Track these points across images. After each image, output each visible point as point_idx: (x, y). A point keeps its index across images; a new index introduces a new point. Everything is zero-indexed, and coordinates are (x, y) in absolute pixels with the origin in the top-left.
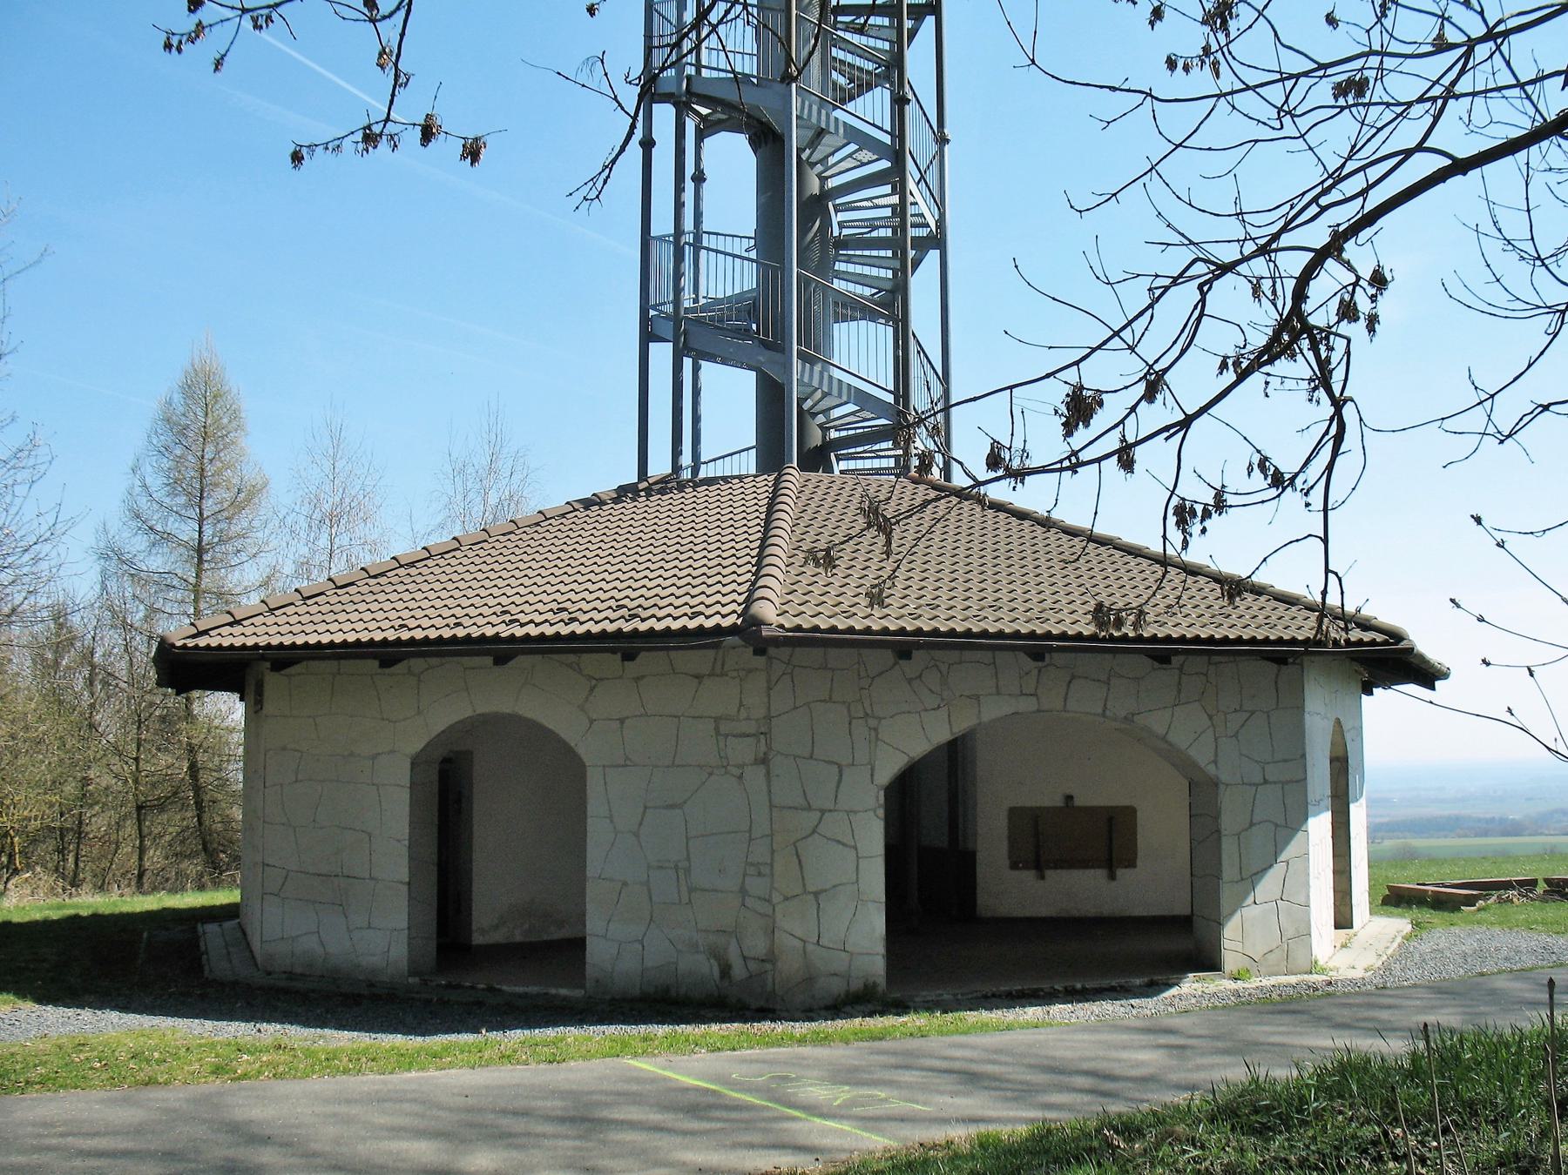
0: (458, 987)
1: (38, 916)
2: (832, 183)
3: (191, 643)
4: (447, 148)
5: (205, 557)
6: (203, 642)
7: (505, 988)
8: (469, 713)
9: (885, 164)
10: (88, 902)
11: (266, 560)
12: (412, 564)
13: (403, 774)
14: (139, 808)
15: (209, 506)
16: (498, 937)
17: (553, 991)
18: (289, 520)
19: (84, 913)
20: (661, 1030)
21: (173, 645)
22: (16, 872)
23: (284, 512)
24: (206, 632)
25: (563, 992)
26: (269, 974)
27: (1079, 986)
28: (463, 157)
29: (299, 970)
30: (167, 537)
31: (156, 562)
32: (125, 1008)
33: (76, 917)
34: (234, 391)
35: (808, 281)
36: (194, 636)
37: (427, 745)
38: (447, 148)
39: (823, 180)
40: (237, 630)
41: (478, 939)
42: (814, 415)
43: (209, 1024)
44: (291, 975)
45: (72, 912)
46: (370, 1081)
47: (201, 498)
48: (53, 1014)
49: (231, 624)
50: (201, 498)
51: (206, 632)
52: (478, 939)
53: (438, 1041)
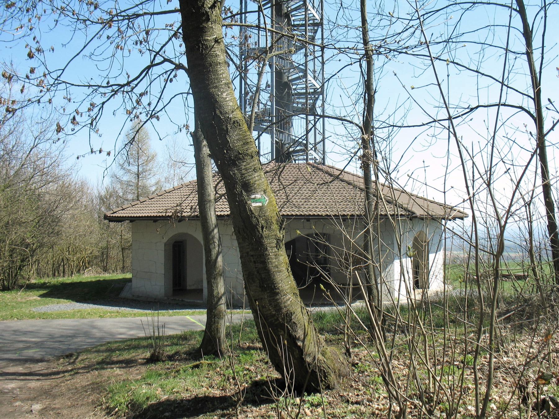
0: (175, 300)
1: (89, 280)
2: (290, 78)
3: (111, 215)
4: (104, 154)
5: (140, 176)
6: (114, 215)
7: (186, 300)
8: (177, 233)
9: (301, 74)
10: (107, 276)
11: (157, 177)
12: (169, 192)
13: (162, 247)
14: (122, 249)
15: (141, 161)
16: (193, 288)
17: (196, 301)
18: (162, 166)
19: (101, 279)
20: (198, 310)
21: (107, 216)
22: (86, 268)
23: (161, 163)
24: (116, 212)
25: (198, 301)
26: (133, 296)
27: (326, 303)
28: (107, 155)
29: (140, 295)
30: (129, 171)
31: (125, 178)
32: (94, 304)
33: (99, 281)
34: (146, 128)
35: (279, 110)
36: (113, 213)
37: (168, 240)
38: (104, 154)
39: (288, 77)
40: (124, 211)
41: (188, 288)
42: (285, 144)
43: (111, 307)
44: (138, 296)
45: (98, 279)
46: (130, 319)
47: (138, 159)
48: (78, 304)
49: (122, 210)
50: (138, 159)
51: (116, 212)
52: (188, 288)
53: (136, 311)
